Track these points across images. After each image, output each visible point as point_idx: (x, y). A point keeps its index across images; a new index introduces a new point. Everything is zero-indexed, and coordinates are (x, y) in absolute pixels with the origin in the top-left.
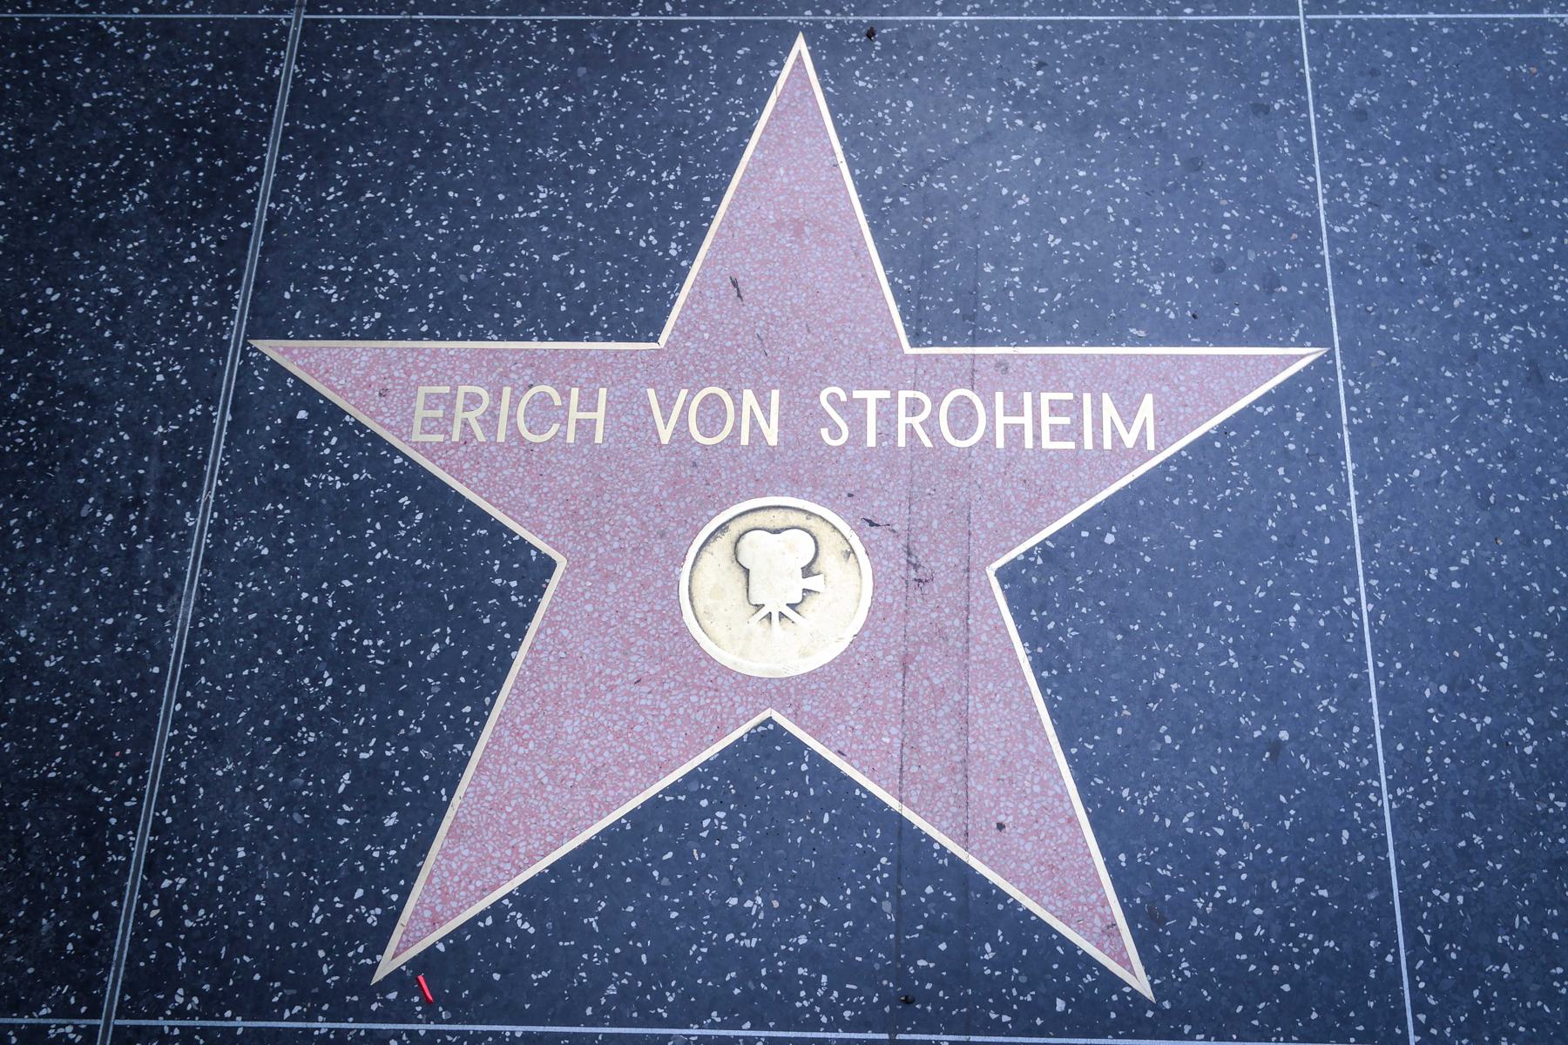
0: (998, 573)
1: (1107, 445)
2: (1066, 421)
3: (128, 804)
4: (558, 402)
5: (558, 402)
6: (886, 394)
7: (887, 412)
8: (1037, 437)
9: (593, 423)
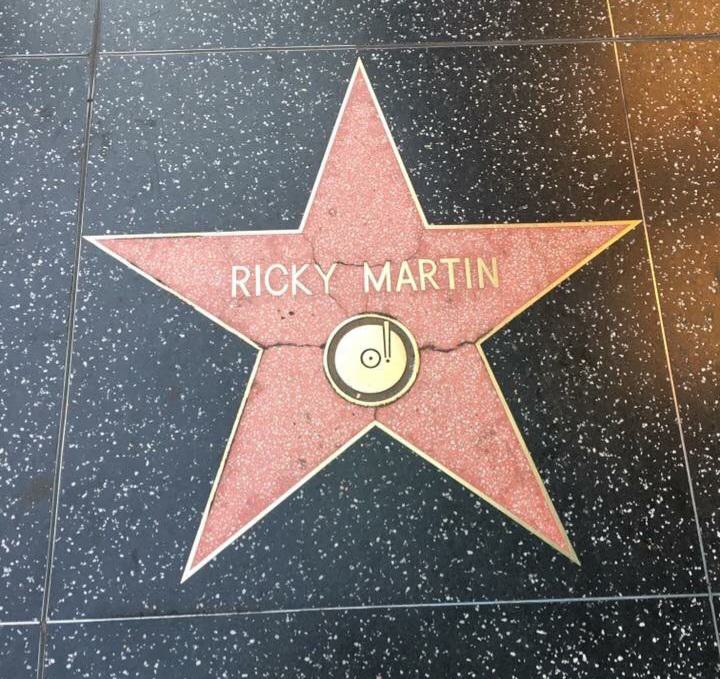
1: (482, 285)
4: (286, 273)
5: (286, 273)
6: (457, 260)
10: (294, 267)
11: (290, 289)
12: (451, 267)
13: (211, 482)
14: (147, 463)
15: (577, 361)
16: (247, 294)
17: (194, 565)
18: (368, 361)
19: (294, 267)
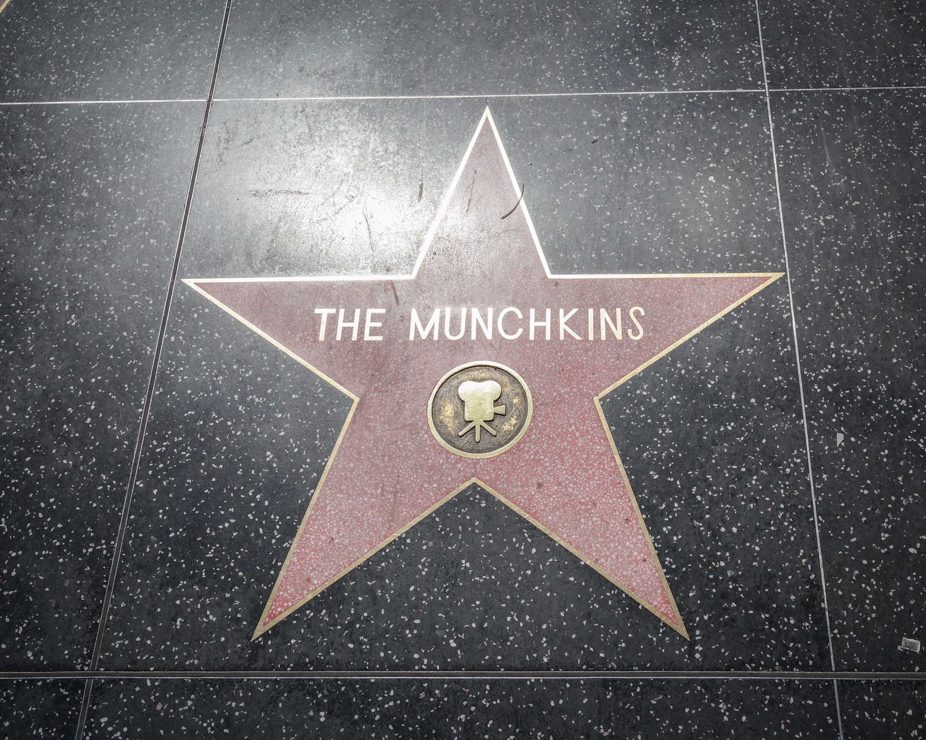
1: (603, 337)
4: (520, 316)
5: (520, 316)
6: (333, 311)
7: (333, 319)
9: (351, 329)
10: (562, 311)
11: (527, 330)
12: (324, 319)
13: (582, 563)
15: (875, 409)
19: (562, 311)
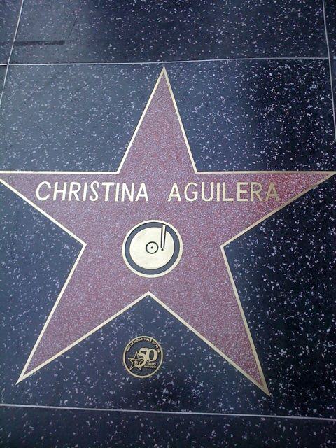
0: (224, 248)
2: (246, 192)
3: (67, 401)
4: (50, 187)
5: (50, 187)
6: (113, 184)
8: (221, 196)
14: (275, 347)
16: (78, 199)
17: (28, 371)
18: (150, 250)
